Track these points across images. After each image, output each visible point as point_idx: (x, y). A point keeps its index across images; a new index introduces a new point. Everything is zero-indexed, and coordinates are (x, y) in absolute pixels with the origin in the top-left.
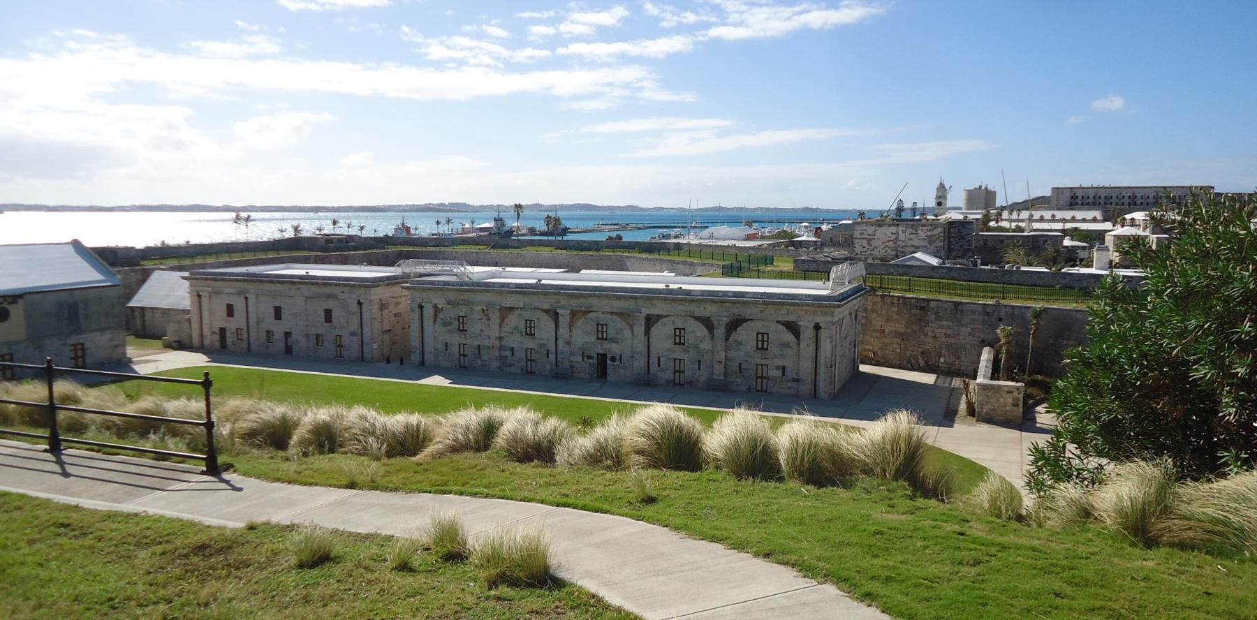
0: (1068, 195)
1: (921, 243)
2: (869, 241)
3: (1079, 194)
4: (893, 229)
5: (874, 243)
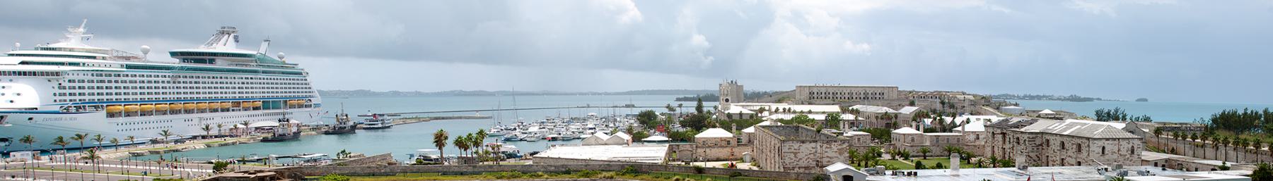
0: (807, 91)
1: (834, 155)
2: (795, 154)
3: (815, 90)
4: (813, 145)
5: (800, 156)
